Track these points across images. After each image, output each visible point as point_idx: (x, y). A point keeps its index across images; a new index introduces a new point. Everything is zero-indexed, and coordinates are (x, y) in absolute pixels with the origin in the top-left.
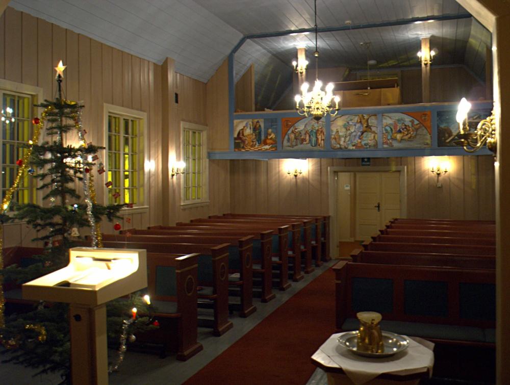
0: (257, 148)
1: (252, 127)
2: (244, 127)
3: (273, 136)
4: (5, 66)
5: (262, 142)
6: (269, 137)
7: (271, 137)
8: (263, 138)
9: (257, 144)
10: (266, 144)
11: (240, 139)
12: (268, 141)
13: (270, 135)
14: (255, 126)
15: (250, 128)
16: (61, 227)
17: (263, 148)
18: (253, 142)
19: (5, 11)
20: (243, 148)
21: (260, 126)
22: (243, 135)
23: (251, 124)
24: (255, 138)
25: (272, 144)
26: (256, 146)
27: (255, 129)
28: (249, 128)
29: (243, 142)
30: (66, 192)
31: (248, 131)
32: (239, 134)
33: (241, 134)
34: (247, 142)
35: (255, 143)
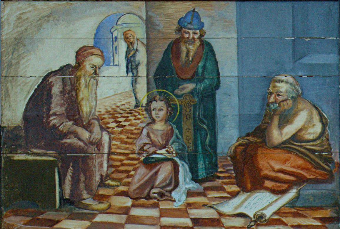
0: (182, 212)
1: (142, 56)
2: (81, 54)
3: (305, 123)
4: (229, 77)
5: (225, 167)
6: (279, 135)
7: (289, 130)
8: (229, 136)
9: (186, 182)
10: (249, 177)
11: (53, 138)
12: (271, 164)
13: (286, 119)
14: (174, 49)
15: (132, 66)
16: (82, 144)
17: (228, 208)
18: (150, 163)
19: (99, 29)
20: (73, 205)
21: (207, 49)
22: (73, 112)
23: (140, 33)
24: (168, 136)
25: (300, 180)
26: (179, 197)
27: (166, 75)
28: (121, 59)
29: (78, 161)
30: (197, 84)
31: (112, 88)
32: (41, 95)
33: (57, 106)
34: (101, 166)
35: (164, 172)
